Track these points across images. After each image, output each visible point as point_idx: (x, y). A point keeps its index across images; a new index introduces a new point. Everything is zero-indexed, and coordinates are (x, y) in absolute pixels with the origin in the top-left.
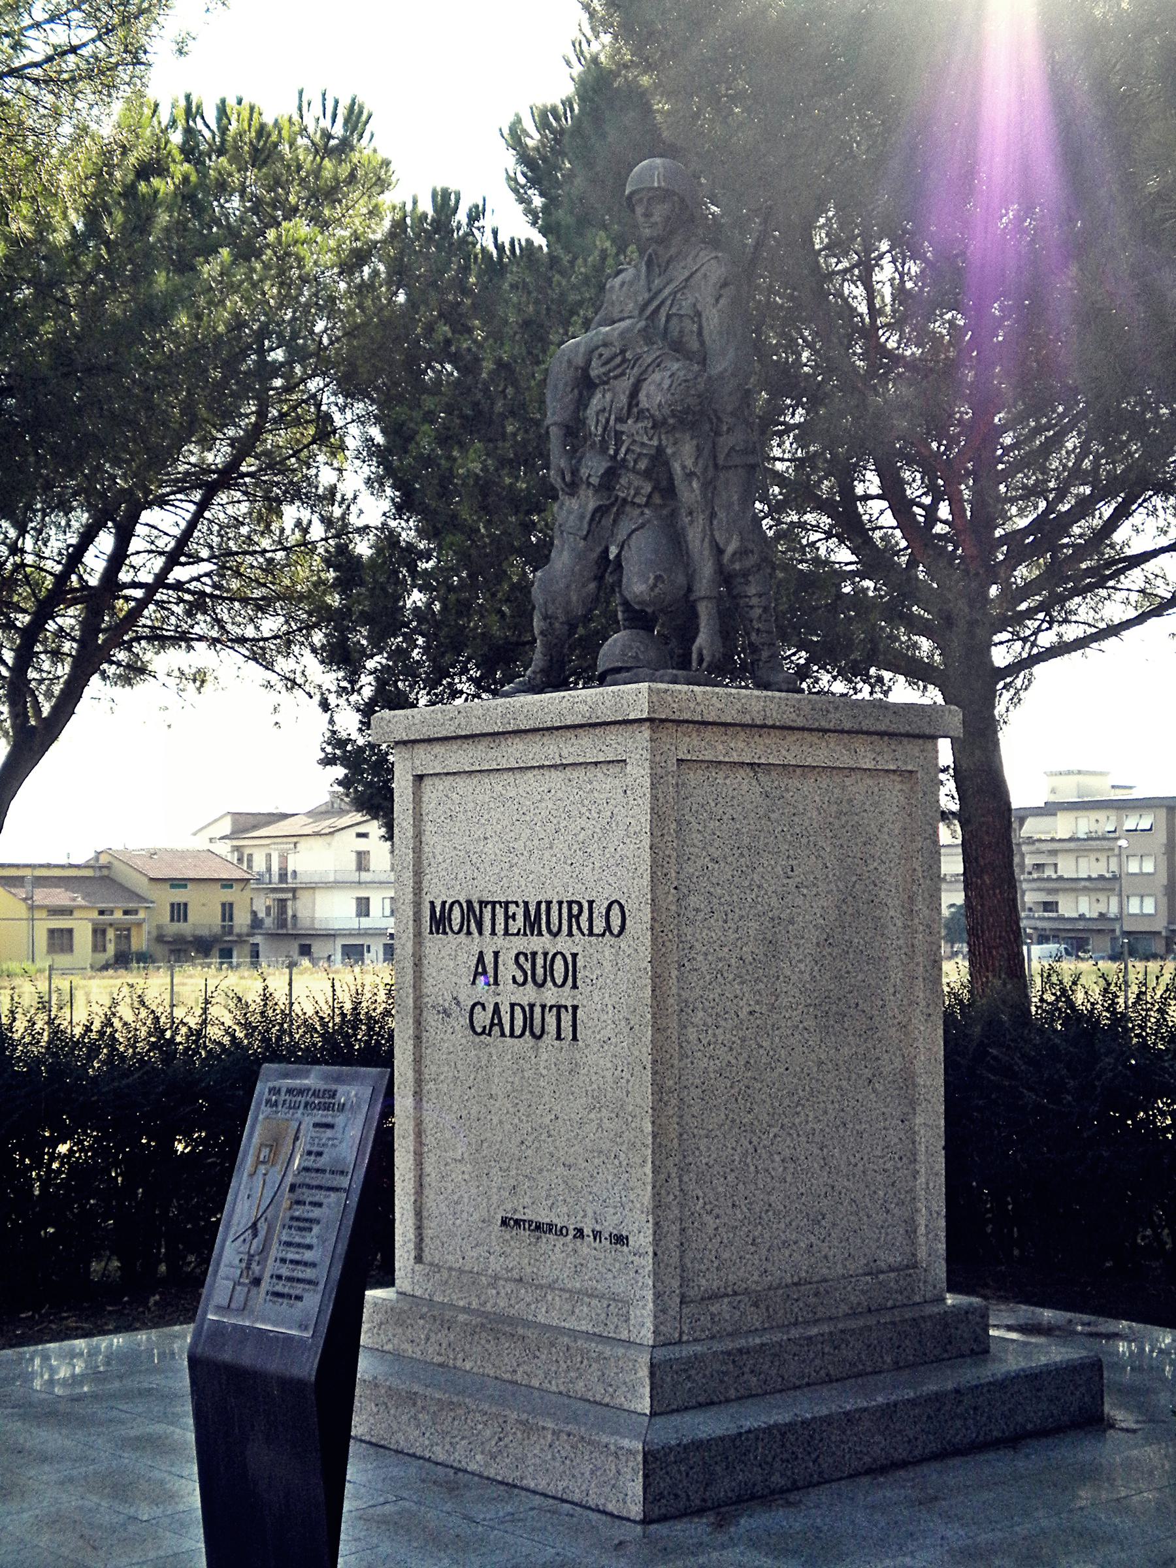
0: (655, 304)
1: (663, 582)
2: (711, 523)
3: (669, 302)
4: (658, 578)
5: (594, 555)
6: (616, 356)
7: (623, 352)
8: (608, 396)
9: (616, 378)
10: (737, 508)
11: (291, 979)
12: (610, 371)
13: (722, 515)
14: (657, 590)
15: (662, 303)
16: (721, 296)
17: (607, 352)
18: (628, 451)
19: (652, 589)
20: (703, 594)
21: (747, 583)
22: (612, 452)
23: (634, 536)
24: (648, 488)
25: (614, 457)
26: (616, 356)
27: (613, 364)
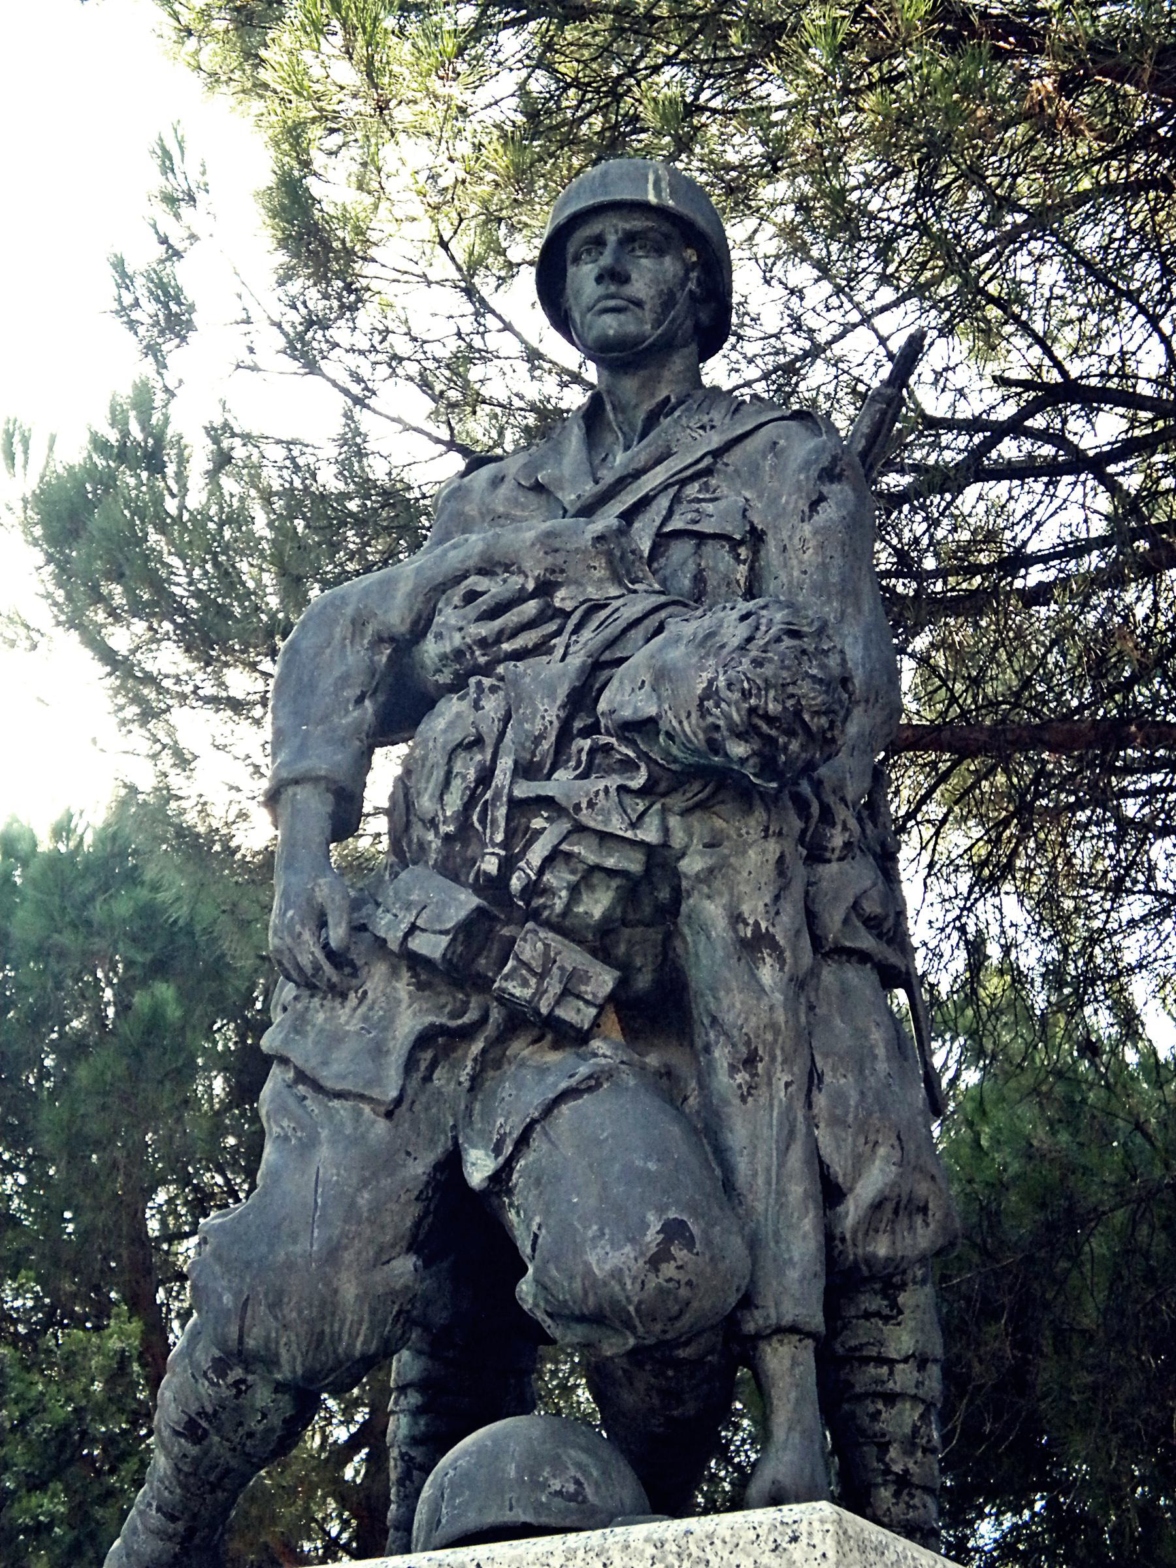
0: (628, 499)
1: (690, 1243)
2: (809, 1105)
3: (664, 502)
4: (674, 1231)
5: (419, 1168)
6: (521, 597)
7: (545, 588)
8: (492, 705)
9: (518, 655)
10: (882, 1067)
11: (51, 449)
12: (500, 637)
13: (836, 1079)
14: (668, 1269)
15: (644, 502)
16: (822, 498)
17: (494, 588)
18: (552, 859)
19: (655, 1262)
20: (790, 1312)
21: (893, 1314)
22: (490, 865)
23: (565, 1109)
24: (603, 981)
25: (494, 887)
26: (521, 597)
27: (512, 618)
